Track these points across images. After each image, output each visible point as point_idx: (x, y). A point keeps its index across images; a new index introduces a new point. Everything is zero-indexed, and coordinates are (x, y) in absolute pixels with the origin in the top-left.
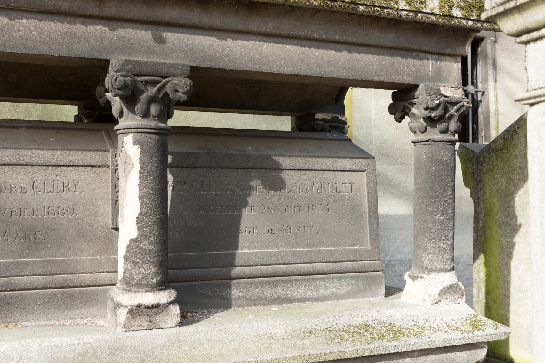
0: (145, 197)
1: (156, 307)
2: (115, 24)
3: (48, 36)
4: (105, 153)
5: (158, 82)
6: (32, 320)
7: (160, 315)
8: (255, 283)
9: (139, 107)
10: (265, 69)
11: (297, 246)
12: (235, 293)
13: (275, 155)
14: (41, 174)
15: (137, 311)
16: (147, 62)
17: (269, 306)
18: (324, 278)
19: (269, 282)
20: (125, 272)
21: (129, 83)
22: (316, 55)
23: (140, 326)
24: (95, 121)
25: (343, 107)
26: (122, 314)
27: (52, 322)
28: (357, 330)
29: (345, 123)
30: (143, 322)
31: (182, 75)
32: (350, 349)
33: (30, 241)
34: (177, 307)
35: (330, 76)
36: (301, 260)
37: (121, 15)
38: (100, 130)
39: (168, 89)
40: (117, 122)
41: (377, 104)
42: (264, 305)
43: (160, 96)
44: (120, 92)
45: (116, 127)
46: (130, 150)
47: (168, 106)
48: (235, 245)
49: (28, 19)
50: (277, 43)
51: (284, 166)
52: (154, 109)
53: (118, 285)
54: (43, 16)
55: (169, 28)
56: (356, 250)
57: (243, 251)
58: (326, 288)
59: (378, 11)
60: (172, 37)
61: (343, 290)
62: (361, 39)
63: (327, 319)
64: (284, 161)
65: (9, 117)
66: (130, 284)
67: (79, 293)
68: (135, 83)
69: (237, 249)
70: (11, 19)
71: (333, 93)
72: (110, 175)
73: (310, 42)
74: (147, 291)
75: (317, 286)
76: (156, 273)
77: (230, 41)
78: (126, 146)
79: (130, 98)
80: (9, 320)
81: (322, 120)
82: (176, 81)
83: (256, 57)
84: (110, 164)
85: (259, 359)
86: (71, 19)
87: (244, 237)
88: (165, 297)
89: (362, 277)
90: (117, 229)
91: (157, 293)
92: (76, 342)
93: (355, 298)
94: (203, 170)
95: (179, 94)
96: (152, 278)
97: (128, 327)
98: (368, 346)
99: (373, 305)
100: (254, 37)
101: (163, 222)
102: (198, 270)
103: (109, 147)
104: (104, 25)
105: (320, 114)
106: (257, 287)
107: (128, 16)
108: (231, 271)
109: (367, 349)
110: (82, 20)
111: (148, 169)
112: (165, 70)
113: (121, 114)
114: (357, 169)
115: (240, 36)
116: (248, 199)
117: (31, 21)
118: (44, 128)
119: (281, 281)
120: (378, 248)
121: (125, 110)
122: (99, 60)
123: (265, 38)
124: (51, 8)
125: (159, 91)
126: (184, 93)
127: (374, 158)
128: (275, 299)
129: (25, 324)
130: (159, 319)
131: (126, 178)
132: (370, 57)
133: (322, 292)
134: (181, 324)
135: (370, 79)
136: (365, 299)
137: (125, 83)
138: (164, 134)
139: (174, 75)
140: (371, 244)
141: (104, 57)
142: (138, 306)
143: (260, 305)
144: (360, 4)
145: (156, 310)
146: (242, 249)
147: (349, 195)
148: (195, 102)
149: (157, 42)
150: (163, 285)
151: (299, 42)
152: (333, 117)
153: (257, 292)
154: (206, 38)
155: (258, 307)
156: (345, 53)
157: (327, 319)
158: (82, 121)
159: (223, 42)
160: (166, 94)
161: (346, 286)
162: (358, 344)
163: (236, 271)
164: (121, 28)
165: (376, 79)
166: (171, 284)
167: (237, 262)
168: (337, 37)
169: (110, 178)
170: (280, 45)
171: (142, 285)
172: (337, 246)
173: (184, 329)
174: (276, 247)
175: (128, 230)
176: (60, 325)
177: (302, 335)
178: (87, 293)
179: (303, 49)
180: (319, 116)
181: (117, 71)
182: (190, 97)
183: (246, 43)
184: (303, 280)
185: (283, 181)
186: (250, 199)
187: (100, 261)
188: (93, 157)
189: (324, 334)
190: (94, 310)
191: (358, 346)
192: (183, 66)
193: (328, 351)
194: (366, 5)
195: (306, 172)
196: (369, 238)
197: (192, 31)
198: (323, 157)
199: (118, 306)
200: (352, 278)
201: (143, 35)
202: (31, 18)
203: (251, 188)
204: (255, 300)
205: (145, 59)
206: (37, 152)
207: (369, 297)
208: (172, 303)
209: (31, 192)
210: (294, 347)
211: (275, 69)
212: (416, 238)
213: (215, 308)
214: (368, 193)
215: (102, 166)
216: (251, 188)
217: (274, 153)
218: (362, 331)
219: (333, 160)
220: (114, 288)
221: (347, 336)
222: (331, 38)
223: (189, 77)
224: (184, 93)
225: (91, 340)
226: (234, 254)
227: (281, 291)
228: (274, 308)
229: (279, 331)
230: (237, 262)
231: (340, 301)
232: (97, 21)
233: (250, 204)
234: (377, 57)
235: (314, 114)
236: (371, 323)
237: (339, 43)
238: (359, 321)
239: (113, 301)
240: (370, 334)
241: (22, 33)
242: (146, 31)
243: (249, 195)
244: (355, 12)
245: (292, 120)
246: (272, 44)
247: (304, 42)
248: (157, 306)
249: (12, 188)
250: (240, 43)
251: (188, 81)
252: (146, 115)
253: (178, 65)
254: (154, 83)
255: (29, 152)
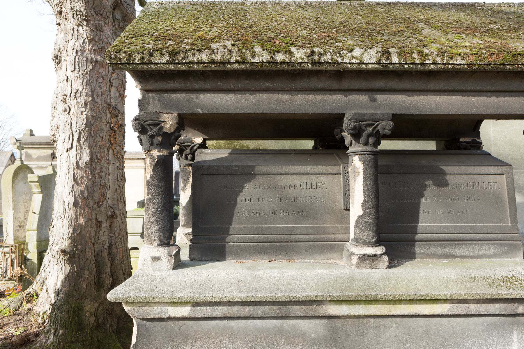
0: (366, 191)
1: (374, 257)
2: (347, 93)
3: (312, 103)
4: (339, 167)
5: (373, 125)
6: (302, 259)
7: (377, 261)
8: (430, 245)
9: (362, 140)
10: (439, 112)
11: (458, 222)
12: (418, 250)
13: (441, 165)
14: (305, 179)
15: (363, 258)
16: (367, 113)
17: (440, 260)
18: (477, 244)
19: (440, 244)
20: (355, 234)
21: (357, 126)
22: (473, 101)
23: (365, 267)
24: (325, 149)
25: (479, 133)
26: (355, 259)
27: (313, 261)
28: (508, 280)
29: (481, 143)
30: (367, 264)
31: (387, 119)
32: (506, 292)
33: (300, 215)
34: (387, 257)
35: (483, 113)
36: (461, 231)
37: (351, 88)
38: (332, 154)
39: (379, 128)
40: (347, 148)
41: (495, 130)
42: (436, 258)
43: (374, 132)
44: (352, 132)
45: (348, 152)
46: (357, 164)
47: (379, 137)
48: (417, 221)
49: (301, 94)
50: (446, 96)
51: (447, 172)
52: (371, 140)
53: (350, 241)
54: (309, 92)
55: (379, 93)
56: (500, 226)
57: (422, 225)
58: (479, 250)
59: (521, 68)
60: (380, 98)
61: (492, 252)
62: (506, 88)
63: (486, 271)
64: (447, 169)
65: (274, 149)
66: (358, 242)
67: (326, 245)
68: (360, 126)
69: (418, 223)
70: (292, 96)
71: (474, 123)
72: (342, 179)
73: (469, 93)
74: (369, 246)
75: (473, 249)
76: (374, 236)
77: (416, 97)
78: (354, 162)
79: (357, 135)
80: (290, 258)
81: (465, 142)
82: (384, 123)
83: (433, 105)
84: (342, 172)
85: (442, 293)
86: (323, 92)
87: (422, 215)
88: (379, 250)
89: (505, 244)
90: (348, 210)
91: (375, 248)
92: (330, 273)
93: (500, 258)
94: (396, 175)
95: (386, 131)
96: (372, 239)
97: (358, 267)
98: (520, 292)
99: (517, 264)
100: (431, 93)
101: (377, 207)
102: (394, 235)
103: (340, 163)
104: (341, 94)
105: (463, 139)
106: (432, 247)
107: (355, 88)
108: (415, 236)
109: (519, 294)
110: (329, 92)
111: (368, 175)
112: (377, 117)
113: (351, 144)
114: (499, 173)
115: (422, 93)
116: (424, 192)
117: (302, 96)
118: (303, 154)
119: (449, 244)
120: (516, 225)
121: (354, 142)
122: (339, 114)
123: (438, 93)
124: (313, 87)
125: (373, 129)
126: (389, 130)
127: (511, 166)
128: (444, 255)
129: (298, 261)
130: (376, 263)
131: (355, 180)
132: (513, 99)
133: (476, 253)
134: (389, 267)
135: (513, 113)
136: (508, 259)
137: (355, 126)
138: (378, 155)
139: (383, 120)
140: (511, 223)
141: (342, 112)
142: (364, 255)
143: (434, 258)
144: (508, 65)
145: (374, 258)
146: (421, 223)
147: (493, 190)
148: (394, 135)
149: (372, 101)
150: (378, 243)
151: (461, 93)
152: (472, 140)
153: (432, 250)
154: (401, 96)
155: (433, 260)
156: (494, 98)
157: (486, 271)
158: (318, 149)
159: (411, 98)
160: (378, 131)
161: (494, 250)
162: (512, 290)
163: (418, 237)
164: (351, 95)
165: (517, 113)
166: (381, 243)
167: (418, 231)
168: (489, 88)
169: (342, 181)
170: (448, 97)
171: (366, 243)
172: (486, 223)
173: (391, 270)
174: (443, 223)
175: (356, 209)
176: (316, 263)
177: (469, 280)
178: (335, 246)
179: (464, 98)
180: (461, 140)
181: (350, 120)
182: (392, 132)
183: (426, 97)
184: (463, 244)
185: (447, 181)
186: (425, 193)
187: (337, 228)
188: (332, 169)
189: (484, 280)
190: (335, 255)
191: (511, 291)
192: (388, 114)
193: (489, 292)
194: (512, 65)
195: (460, 175)
196: (509, 219)
197: (382, 93)
198: (474, 166)
199: (353, 254)
200: (498, 245)
201: (363, 98)
202: (302, 94)
203: (426, 186)
204: (431, 255)
205: (365, 112)
206: (302, 167)
207: (511, 258)
208: (383, 254)
209: (300, 189)
210: (465, 288)
211: (445, 112)
212: (55, 173)
213: (406, 258)
214: (508, 189)
215: (337, 174)
216: (426, 186)
217: (440, 164)
218: (513, 281)
219: (481, 167)
220: (348, 243)
221: (502, 284)
222: (484, 89)
223: (391, 120)
224: (389, 130)
225: (338, 273)
226: (417, 226)
227: (447, 250)
228: (445, 261)
229: (452, 276)
230: (419, 231)
231: (490, 259)
232: (337, 92)
233: (426, 195)
234: (518, 98)
235: (459, 139)
236: (519, 276)
237: (489, 91)
238: (510, 274)
239: (348, 251)
240: (520, 284)
241: (298, 103)
242: (365, 95)
243: (425, 190)
244: (503, 70)
245: (436, 143)
246: (443, 96)
247: (465, 93)
248: (375, 255)
249: (290, 186)
250: (422, 97)
251: (392, 123)
252: (366, 144)
253: (385, 113)
254: (371, 125)
255: (298, 167)
